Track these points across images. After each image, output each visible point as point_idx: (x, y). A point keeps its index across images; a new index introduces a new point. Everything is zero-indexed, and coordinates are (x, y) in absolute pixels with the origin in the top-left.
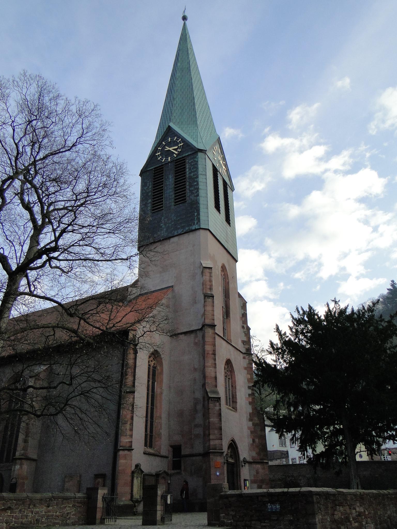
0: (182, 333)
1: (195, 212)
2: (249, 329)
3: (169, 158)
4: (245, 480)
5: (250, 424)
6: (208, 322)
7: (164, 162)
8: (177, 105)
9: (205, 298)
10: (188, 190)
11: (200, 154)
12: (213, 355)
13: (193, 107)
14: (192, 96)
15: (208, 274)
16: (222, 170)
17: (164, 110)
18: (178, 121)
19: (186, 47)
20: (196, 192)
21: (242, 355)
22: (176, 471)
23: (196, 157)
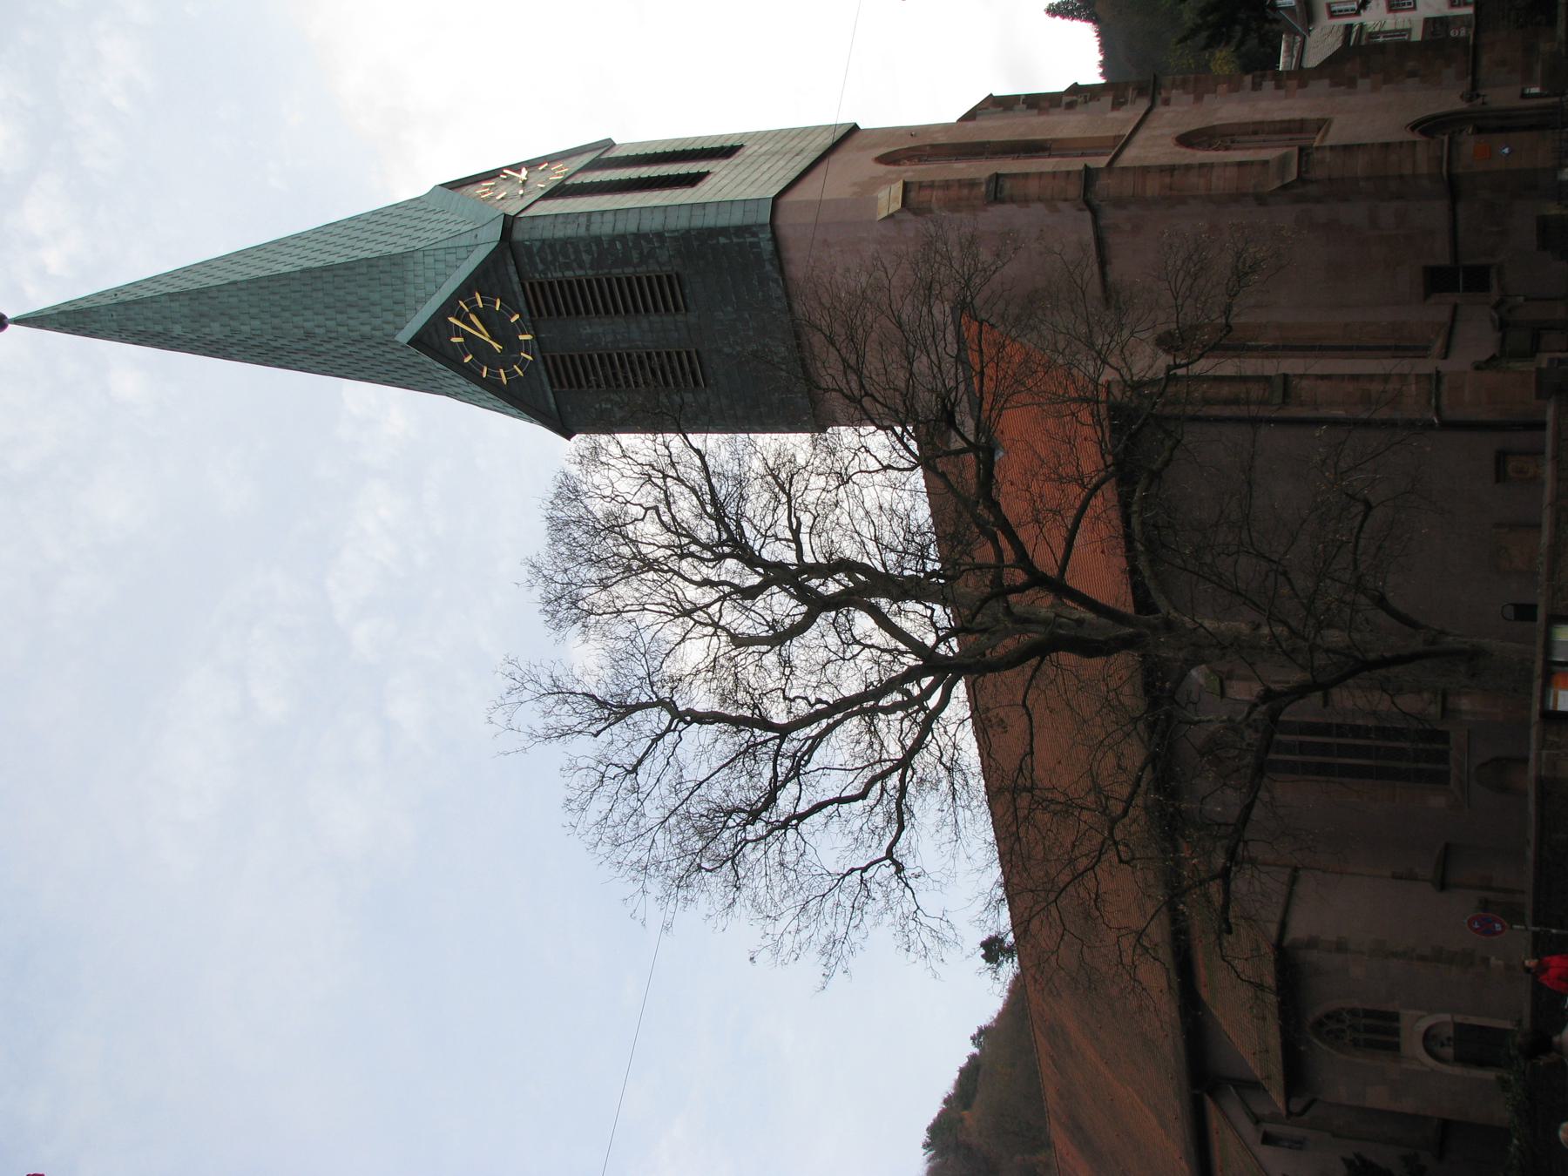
0: (1103, 275)
1: (714, 242)
2: (1075, 89)
3: (522, 337)
4: (1524, 96)
5: (1364, 84)
6: (1074, 190)
7: (532, 356)
8: (330, 324)
9: (1002, 201)
10: (638, 270)
11: (518, 235)
12: (1176, 172)
13: (341, 272)
14: (298, 275)
15: (925, 194)
16: (557, 174)
17: (338, 372)
18: (389, 316)
19: (109, 310)
20: (649, 241)
21: (1160, 109)
22: (1494, 282)
23: (529, 249)
